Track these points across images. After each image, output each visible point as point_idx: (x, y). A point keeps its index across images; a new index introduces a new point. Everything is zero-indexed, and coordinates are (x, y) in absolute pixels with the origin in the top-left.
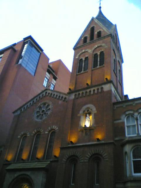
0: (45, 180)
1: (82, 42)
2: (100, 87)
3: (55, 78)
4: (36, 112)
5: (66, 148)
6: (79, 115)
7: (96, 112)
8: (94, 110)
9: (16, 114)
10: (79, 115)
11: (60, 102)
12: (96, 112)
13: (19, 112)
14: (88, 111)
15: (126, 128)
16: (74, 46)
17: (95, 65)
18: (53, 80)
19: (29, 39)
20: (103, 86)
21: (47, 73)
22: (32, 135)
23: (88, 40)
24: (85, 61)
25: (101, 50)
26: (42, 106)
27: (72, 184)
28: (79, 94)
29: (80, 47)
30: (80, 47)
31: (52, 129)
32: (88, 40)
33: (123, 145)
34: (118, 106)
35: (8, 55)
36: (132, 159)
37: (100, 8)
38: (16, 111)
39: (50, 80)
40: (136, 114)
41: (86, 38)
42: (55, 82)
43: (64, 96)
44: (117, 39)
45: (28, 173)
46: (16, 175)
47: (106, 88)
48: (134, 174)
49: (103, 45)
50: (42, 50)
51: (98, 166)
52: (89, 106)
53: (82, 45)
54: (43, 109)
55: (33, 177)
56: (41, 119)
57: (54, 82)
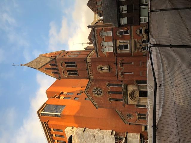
0: (131, 85)
2: (88, 64)
7: (101, 65)
8: (101, 66)
10: (102, 73)
12: (101, 65)
14: (100, 69)
15: (145, 22)
16: (90, 9)
17: (74, 66)
20: (88, 62)
23: (56, 71)
32: (56, 71)
34: (98, 55)
36: (123, 50)
38: (96, 107)
41: (55, 73)
43: (120, 66)
46: (130, 99)
51: (125, 63)
52: (97, 68)
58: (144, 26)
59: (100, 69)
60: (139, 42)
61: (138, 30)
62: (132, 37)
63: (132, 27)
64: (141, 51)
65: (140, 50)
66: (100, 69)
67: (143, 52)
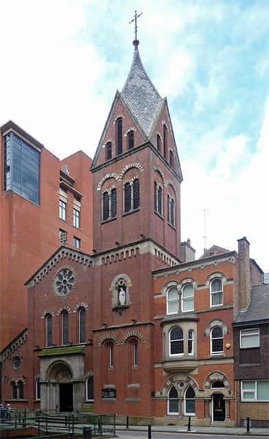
1: (103, 156)
3: (79, 198)
4: (55, 282)
5: (99, 330)
6: (110, 289)
7: (131, 285)
9: (29, 286)
10: (110, 289)
11: (85, 268)
12: (131, 285)
13: (33, 283)
18: (75, 202)
19: (11, 130)
20: (139, 246)
21: (61, 192)
22: (58, 314)
24: (112, 196)
25: (135, 175)
26: (62, 273)
27: (169, 413)
28: (108, 257)
29: (99, 168)
30: (99, 168)
31: (81, 307)
33: (163, 325)
35: (69, 360)
37: (136, 43)
39: (69, 203)
40: (179, 286)
42: (79, 204)
44: (169, 134)
45: (64, 359)
46: (51, 362)
47: (144, 248)
48: (170, 355)
49: (137, 165)
50: (41, 146)
52: (121, 276)
53: (105, 164)
54: (64, 279)
55: (69, 362)
56: (65, 292)
57: (77, 205)
58: (230, 393)
59: (122, 282)
60: (189, 379)
61: (221, 378)
62: (202, 363)
63: (232, 361)
64: (166, 386)
65: (168, 383)
66: (119, 284)
67: (165, 389)
